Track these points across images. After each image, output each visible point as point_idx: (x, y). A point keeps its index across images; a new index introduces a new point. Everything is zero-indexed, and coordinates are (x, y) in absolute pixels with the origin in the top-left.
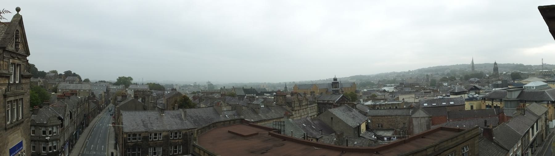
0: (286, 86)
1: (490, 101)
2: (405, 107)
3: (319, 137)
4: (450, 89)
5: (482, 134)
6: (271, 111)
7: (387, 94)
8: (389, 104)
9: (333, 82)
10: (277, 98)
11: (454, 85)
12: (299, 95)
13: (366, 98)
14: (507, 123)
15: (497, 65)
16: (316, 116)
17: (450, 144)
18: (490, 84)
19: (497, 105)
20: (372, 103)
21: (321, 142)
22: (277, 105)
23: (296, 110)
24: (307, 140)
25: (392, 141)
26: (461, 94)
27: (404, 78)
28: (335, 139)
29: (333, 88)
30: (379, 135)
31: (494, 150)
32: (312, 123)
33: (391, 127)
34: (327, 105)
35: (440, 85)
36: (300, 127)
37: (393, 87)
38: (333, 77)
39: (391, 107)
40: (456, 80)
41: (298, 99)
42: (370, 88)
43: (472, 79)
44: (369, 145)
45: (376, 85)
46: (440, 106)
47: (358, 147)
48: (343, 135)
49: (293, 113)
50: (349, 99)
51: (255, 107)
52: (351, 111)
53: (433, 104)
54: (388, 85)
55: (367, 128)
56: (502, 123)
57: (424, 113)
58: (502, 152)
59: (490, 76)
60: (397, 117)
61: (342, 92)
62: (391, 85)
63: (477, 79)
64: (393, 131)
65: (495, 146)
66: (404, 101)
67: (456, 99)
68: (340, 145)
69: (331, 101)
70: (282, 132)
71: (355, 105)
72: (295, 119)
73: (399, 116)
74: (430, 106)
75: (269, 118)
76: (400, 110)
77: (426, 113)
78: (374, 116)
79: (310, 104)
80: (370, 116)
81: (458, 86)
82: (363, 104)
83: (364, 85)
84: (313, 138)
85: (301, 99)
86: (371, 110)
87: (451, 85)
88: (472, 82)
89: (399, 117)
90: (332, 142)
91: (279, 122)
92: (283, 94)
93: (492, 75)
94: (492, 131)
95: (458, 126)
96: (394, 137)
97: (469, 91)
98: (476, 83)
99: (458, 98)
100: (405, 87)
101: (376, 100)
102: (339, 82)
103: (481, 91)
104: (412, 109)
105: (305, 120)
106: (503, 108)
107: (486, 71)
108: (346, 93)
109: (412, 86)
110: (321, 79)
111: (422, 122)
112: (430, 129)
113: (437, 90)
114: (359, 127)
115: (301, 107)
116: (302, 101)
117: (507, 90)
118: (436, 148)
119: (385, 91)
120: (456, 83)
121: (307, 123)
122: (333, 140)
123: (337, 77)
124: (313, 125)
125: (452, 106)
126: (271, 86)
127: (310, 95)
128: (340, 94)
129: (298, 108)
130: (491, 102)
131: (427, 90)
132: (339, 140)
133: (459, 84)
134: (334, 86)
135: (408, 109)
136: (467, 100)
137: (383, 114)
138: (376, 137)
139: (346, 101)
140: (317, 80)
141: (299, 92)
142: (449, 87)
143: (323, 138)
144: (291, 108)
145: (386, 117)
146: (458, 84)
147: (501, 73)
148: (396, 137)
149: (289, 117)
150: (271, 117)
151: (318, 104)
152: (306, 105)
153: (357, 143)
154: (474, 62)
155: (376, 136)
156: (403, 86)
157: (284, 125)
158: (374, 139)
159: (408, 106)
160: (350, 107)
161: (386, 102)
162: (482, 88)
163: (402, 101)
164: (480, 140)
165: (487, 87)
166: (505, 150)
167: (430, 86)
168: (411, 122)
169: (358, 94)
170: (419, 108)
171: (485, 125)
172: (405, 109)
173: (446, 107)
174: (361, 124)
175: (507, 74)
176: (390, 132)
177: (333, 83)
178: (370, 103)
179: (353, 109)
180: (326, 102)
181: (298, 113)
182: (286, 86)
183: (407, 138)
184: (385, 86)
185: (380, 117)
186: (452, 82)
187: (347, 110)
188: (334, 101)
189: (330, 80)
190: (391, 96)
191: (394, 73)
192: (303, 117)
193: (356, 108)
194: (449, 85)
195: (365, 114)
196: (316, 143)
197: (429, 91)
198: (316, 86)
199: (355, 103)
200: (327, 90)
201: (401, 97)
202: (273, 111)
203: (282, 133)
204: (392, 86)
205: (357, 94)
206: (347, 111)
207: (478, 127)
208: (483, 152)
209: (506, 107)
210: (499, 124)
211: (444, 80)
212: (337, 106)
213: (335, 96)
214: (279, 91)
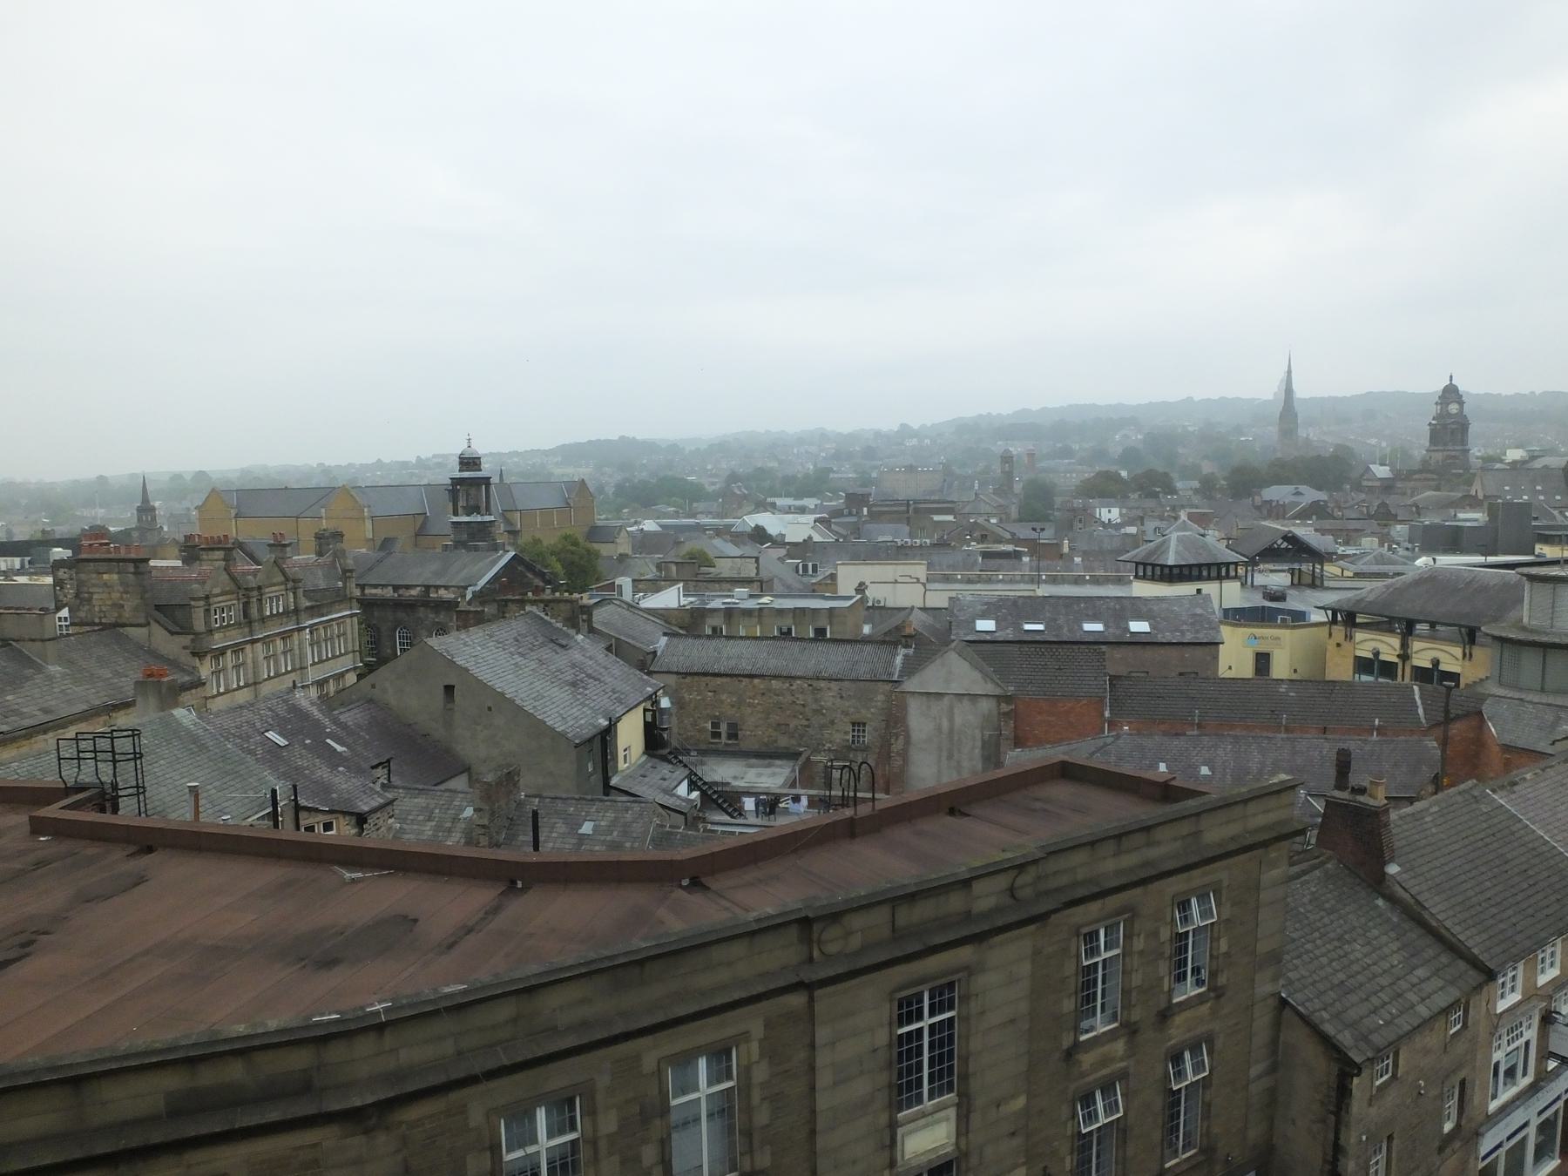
0: (145, 499)
1: (1391, 631)
2: (867, 629)
3: (374, 804)
4: (1136, 541)
5: (1312, 836)
6: (39, 669)
7: (771, 555)
8: (781, 612)
9: (458, 475)
10: (83, 576)
11: (1163, 524)
12: (238, 554)
13: (651, 572)
14: (1502, 787)
15: (1461, 403)
16: (351, 678)
17: (1110, 865)
18: (1399, 527)
19: (1436, 663)
20: (684, 601)
21: (380, 834)
22: (82, 624)
23: (222, 652)
24: (298, 828)
25: (781, 821)
26: (1199, 578)
27: (875, 467)
28: (469, 812)
29: (456, 513)
30: (716, 784)
31: (1386, 950)
32: (326, 721)
33: (783, 742)
34: (421, 612)
35: (1077, 518)
36: (252, 753)
37: (812, 517)
38: (458, 448)
39: (790, 630)
40: (1173, 491)
41: (233, 578)
42: (676, 515)
43: (1276, 493)
44: (663, 839)
45: (713, 497)
46: (1065, 639)
47: (599, 852)
48: (515, 784)
49: (205, 669)
50: (555, 575)
52: (563, 646)
53: (1028, 627)
54: (780, 502)
55: (654, 739)
56: (1462, 787)
57: (976, 675)
58: (1436, 972)
59: (1398, 476)
60: (823, 684)
61: (514, 533)
62: (799, 503)
63: (1310, 495)
64: (791, 763)
65: (1395, 919)
66: (863, 600)
67: (1164, 606)
68: (498, 845)
69: (446, 588)
70: (123, 802)
71: (587, 610)
72: (218, 704)
73: (830, 680)
74: (1009, 634)
75: (27, 722)
76: (841, 648)
77: (986, 676)
78: (686, 674)
79: (314, 611)
80: (668, 672)
81: (1184, 527)
82: (633, 607)
83: (643, 496)
84: (331, 812)
85: (252, 582)
86: (675, 641)
87: (1142, 519)
88: (1275, 511)
89: (833, 685)
90: (449, 831)
91: (102, 735)
92: (123, 554)
93: (1420, 471)
94: (1386, 825)
95: (1163, 767)
96: (796, 799)
97: (1252, 562)
98: (1304, 515)
99: (1179, 598)
100: (875, 516)
101: (710, 585)
102: (495, 480)
103: (1331, 569)
104: (907, 646)
105: (282, 710)
106: (1480, 690)
107: (1373, 441)
108: (537, 542)
109: (912, 512)
110: (386, 460)
111: (958, 720)
112: (999, 764)
113: (1059, 546)
114: (606, 737)
115: (256, 625)
116: (259, 588)
117: (1526, 570)
118: (1019, 882)
119: (759, 535)
120: (1174, 509)
121: (295, 722)
122: (455, 819)
123: (480, 448)
124: (330, 736)
125: (1139, 642)
126: (24, 502)
127: (313, 556)
128: (495, 548)
129: (237, 637)
130: (1395, 642)
131: (1000, 541)
132: (493, 813)
133: (1191, 517)
134: (460, 504)
135: (883, 642)
136: (1238, 616)
137: (745, 666)
138: (695, 795)
139: (537, 591)
140: (358, 460)
141: (240, 539)
142: (1132, 530)
143: (398, 808)
144: (186, 640)
145: (756, 681)
146: (1183, 516)
147: (1489, 459)
148: (804, 801)
149: (171, 695)
150: (46, 711)
151: (368, 605)
152: (286, 613)
153: (595, 828)
154: (1295, 387)
155: (699, 789)
156: (865, 509)
157: (137, 756)
158: (684, 807)
159: (885, 627)
160: (559, 625)
161: (765, 600)
162: (1341, 549)
163: (850, 598)
164: (1296, 869)
165: (1370, 543)
166: (1462, 965)
167: (1020, 520)
168: (895, 720)
169: (605, 550)
170: (946, 643)
171: (1341, 783)
172: (866, 641)
173: (1104, 648)
174: (619, 719)
175: (1538, 464)
176: (778, 770)
177: (456, 482)
178: (670, 598)
179: (572, 632)
180: (414, 592)
181: (237, 667)
182: (145, 499)
183: (864, 810)
184: (762, 506)
185: (724, 680)
186: (1150, 503)
187: (541, 639)
188: (466, 588)
189: (439, 465)
190: (797, 567)
191: (823, 436)
192: (266, 689)
193: (592, 630)
194: (1131, 523)
195: (645, 663)
196: (357, 842)
197: (1010, 548)
198: (357, 502)
199: (586, 599)
200: (420, 520)
201: (849, 577)
202: (54, 669)
203: (127, 806)
204: (802, 510)
205: (596, 546)
206: (542, 645)
207: (1291, 788)
208: (1309, 946)
209: (1501, 684)
210: (1437, 784)
211: (1105, 487)
212: (479, 619)
213: (464, 556)
214: (97, 537)
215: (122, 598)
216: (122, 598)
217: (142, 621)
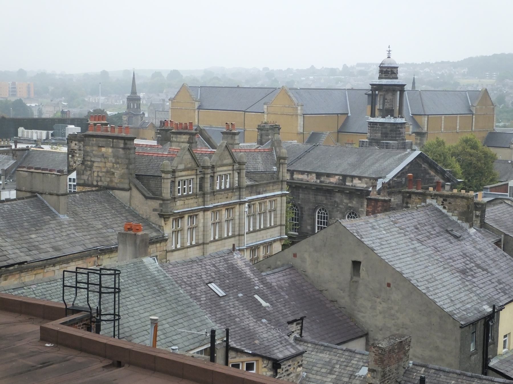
144: (156, 204)
215: (113, 167)
217: (126, 186)
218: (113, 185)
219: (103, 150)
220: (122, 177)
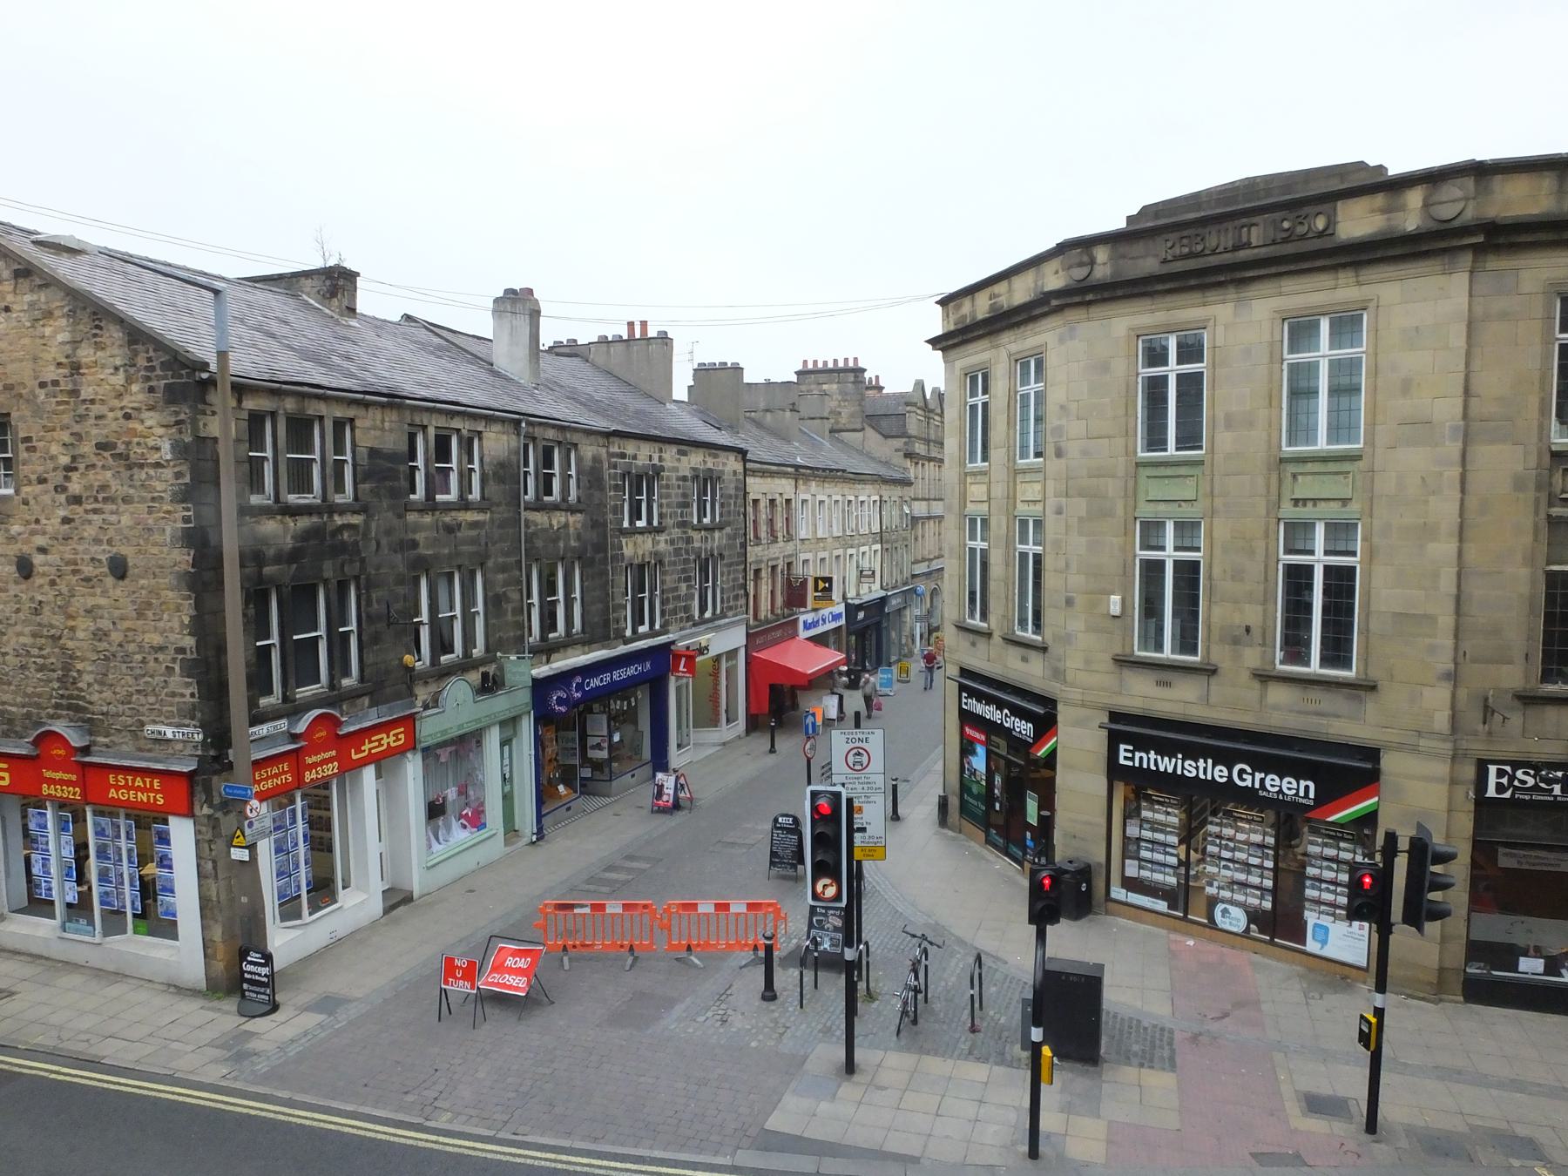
51: (762, 405)
144: (899, 443)
215: (839, 406)
216: (839, 406)
217: (858, 426)
218: (840, 426)
219: (825, 387)
220: (852, 415)
